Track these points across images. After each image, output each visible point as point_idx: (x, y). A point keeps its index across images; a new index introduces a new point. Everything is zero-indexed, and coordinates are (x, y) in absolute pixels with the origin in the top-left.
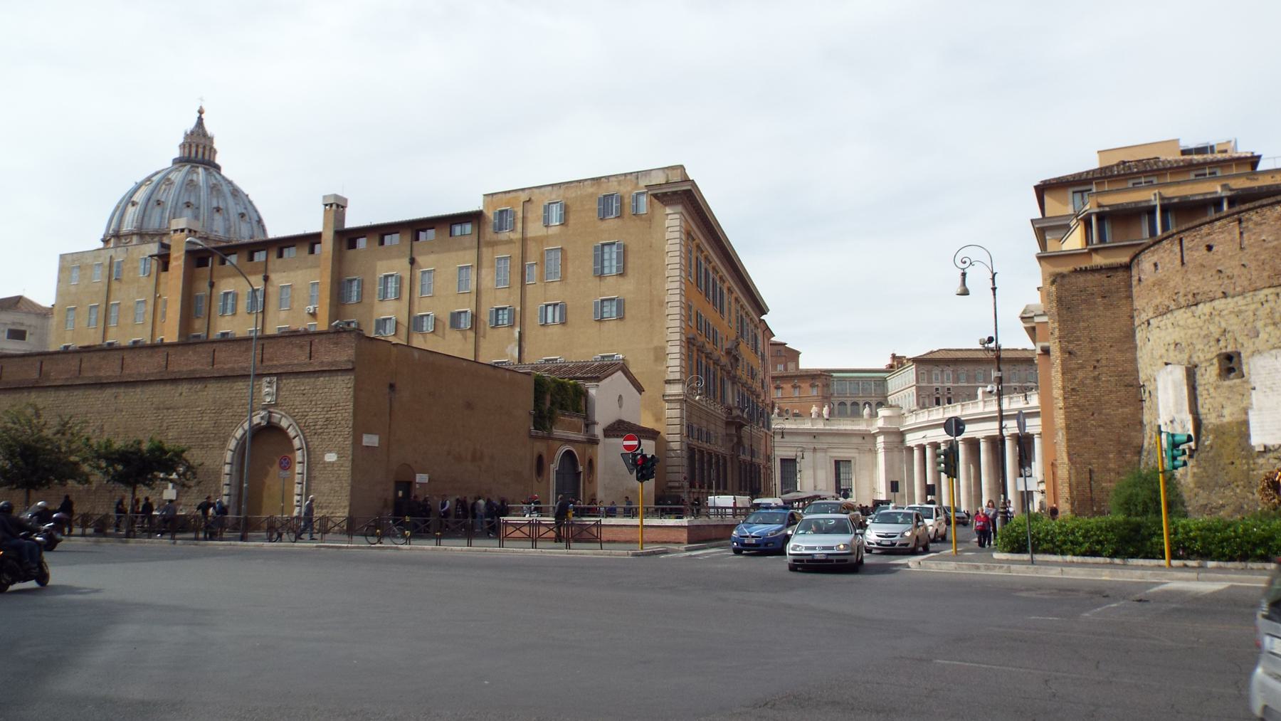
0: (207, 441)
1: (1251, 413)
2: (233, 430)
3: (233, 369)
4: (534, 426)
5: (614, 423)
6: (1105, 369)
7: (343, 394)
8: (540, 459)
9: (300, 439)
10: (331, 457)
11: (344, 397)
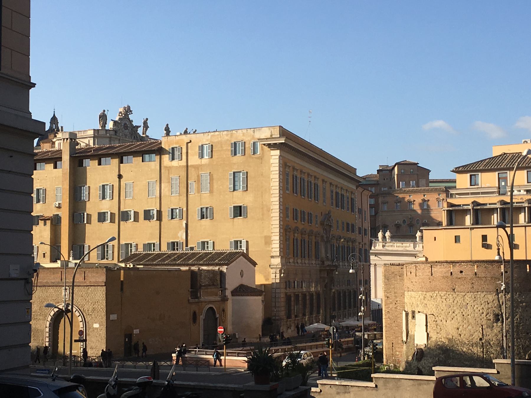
0: (37, 316)
1: (415, 332)
2: (49, 311)
3: (47, 282)
4: (191, 297)
5: (238, 287)
6: (399, 304)
7: (100, 297)
8: (195, 313)
9: (81, 317)
10: (96, 326)
11: (102, 298)
